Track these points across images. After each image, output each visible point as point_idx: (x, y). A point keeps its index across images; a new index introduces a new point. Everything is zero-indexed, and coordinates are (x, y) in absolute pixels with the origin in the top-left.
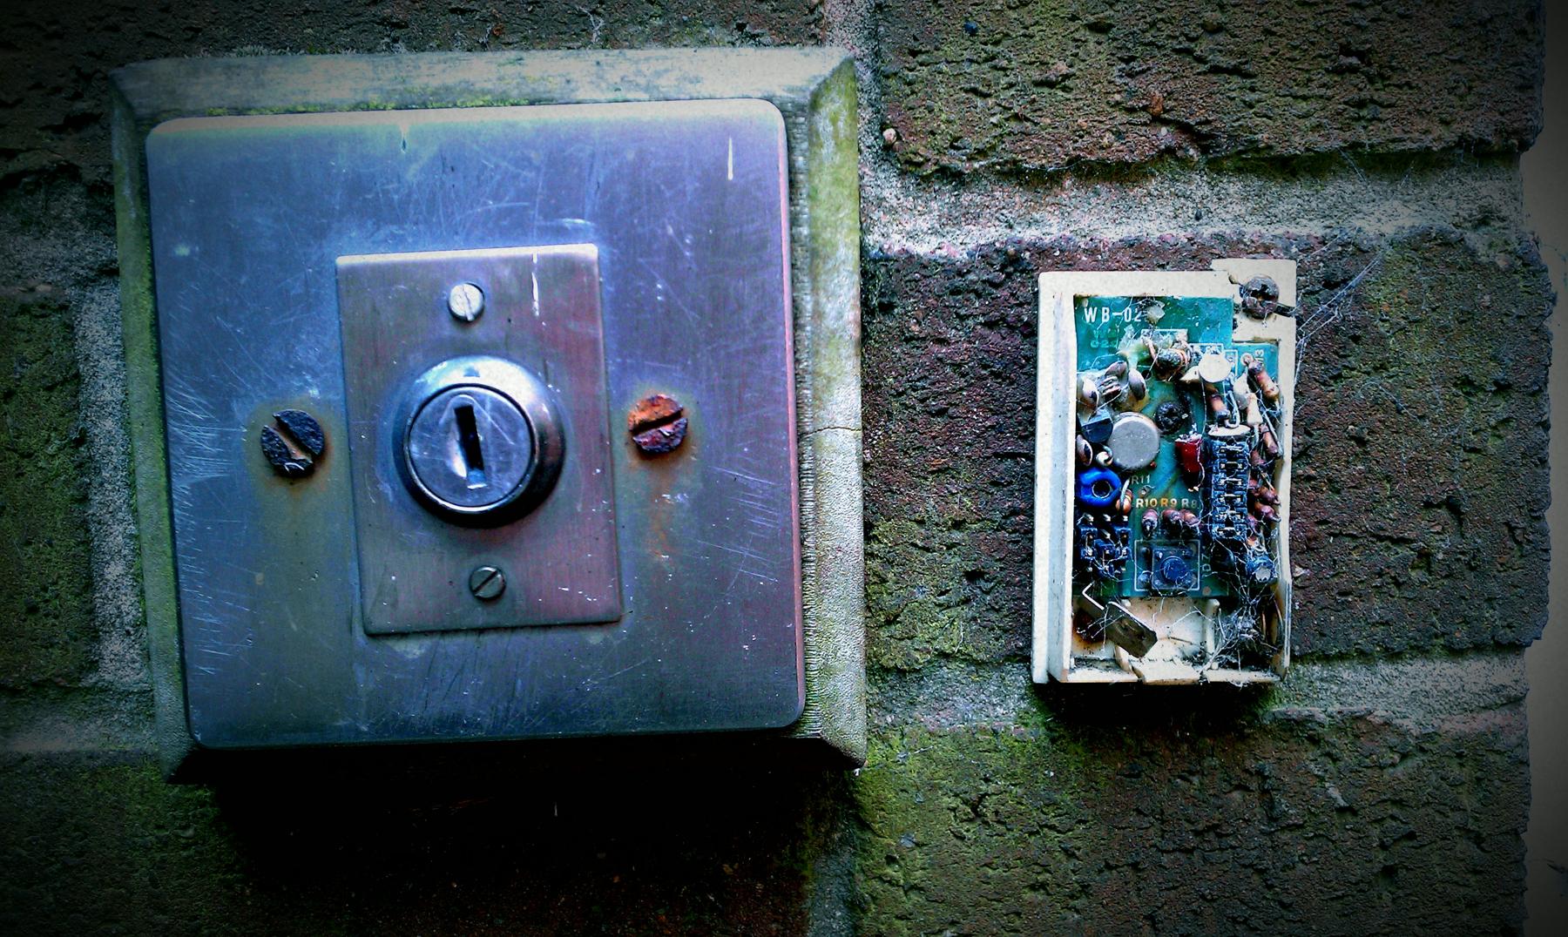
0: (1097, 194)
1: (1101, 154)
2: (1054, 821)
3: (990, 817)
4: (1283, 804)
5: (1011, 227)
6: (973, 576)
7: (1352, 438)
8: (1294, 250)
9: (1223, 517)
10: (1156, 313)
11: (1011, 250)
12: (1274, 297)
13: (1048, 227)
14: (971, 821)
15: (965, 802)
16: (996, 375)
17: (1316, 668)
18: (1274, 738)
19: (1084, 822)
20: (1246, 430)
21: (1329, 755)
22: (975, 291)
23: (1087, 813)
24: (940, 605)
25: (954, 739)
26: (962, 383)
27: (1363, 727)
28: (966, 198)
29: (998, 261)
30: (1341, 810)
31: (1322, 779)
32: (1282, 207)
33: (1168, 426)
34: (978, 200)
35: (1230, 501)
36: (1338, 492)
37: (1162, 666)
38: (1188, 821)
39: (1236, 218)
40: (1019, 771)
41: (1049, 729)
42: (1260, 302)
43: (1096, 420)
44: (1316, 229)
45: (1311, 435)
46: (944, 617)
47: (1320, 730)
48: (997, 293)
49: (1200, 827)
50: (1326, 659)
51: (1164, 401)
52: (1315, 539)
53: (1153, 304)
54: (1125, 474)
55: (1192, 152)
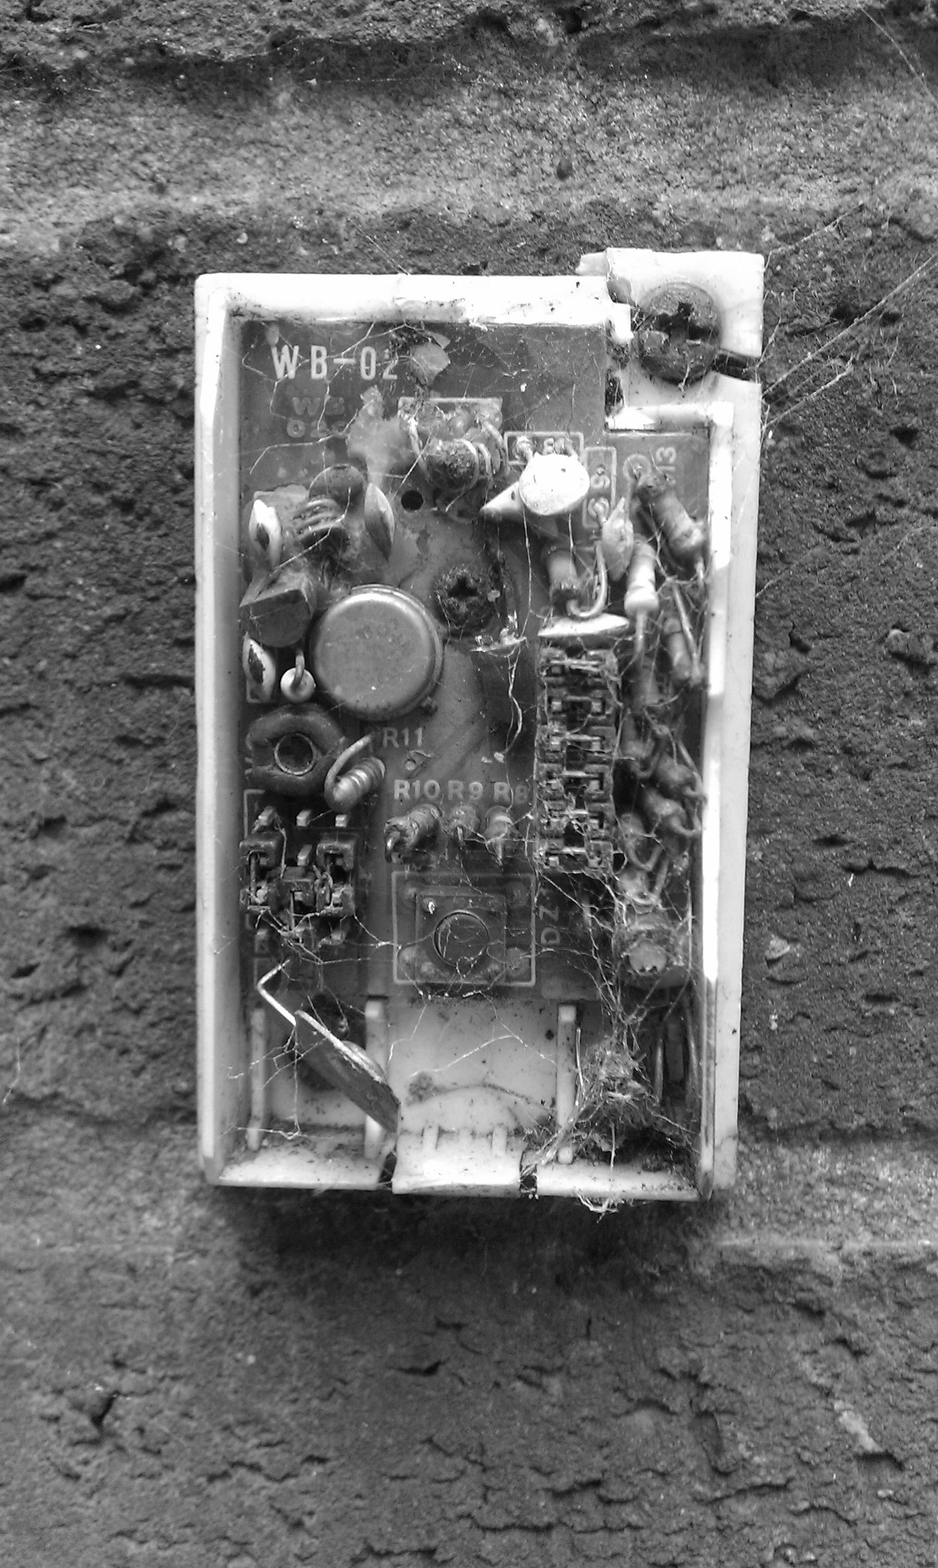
0: (346, 122)
1: (339, 26)
2: (257, 1456)
3: (129, 1437)
4: (741, 1444)
5: (161, 189)
6: (87, 936)
7: (898, 656)
8: (767, 236)
9: (558, 823)
10: (432, 360)
11: (145, 230)
12: (712, 333)
13: (244, 189)
14: (95, 1443)
15: (78, 1407)
16: (126, 506)
17: (820, 1157)
18: (723, 1303)
19: (322, 1460)
20: (613, 623)
21: (843, 1342)
22: (69, 321)
23: (326, 1444)
24: (18, 997)
25: (48, 1275)
26: (52, 522)
27: (918, 1287)
28: (67, 129)
29: (121, 257)
30: (869, 1459)
31: (827, 1393)
32: (751, 149)
33: (456, 618)
34: (92, 132)
35: (572, 785)
36: (866, 777)
37: (453, 1160)
38: (537, 1469)
39: (647, 175)
40: (182, 1350)
41: (244, 1265)
42: (680, 341)
43: (273, 593)
44: (822, 195)
45: (804, 650)
46: (28, 1021)
47: (822, 1291)
48: (118, 325)
49: (562, 1483)
50: (839, 1137)
51: (452, 562)
52: (814, 877)
53: (422, 341)
54: (353, 723)
55: (542, 25)
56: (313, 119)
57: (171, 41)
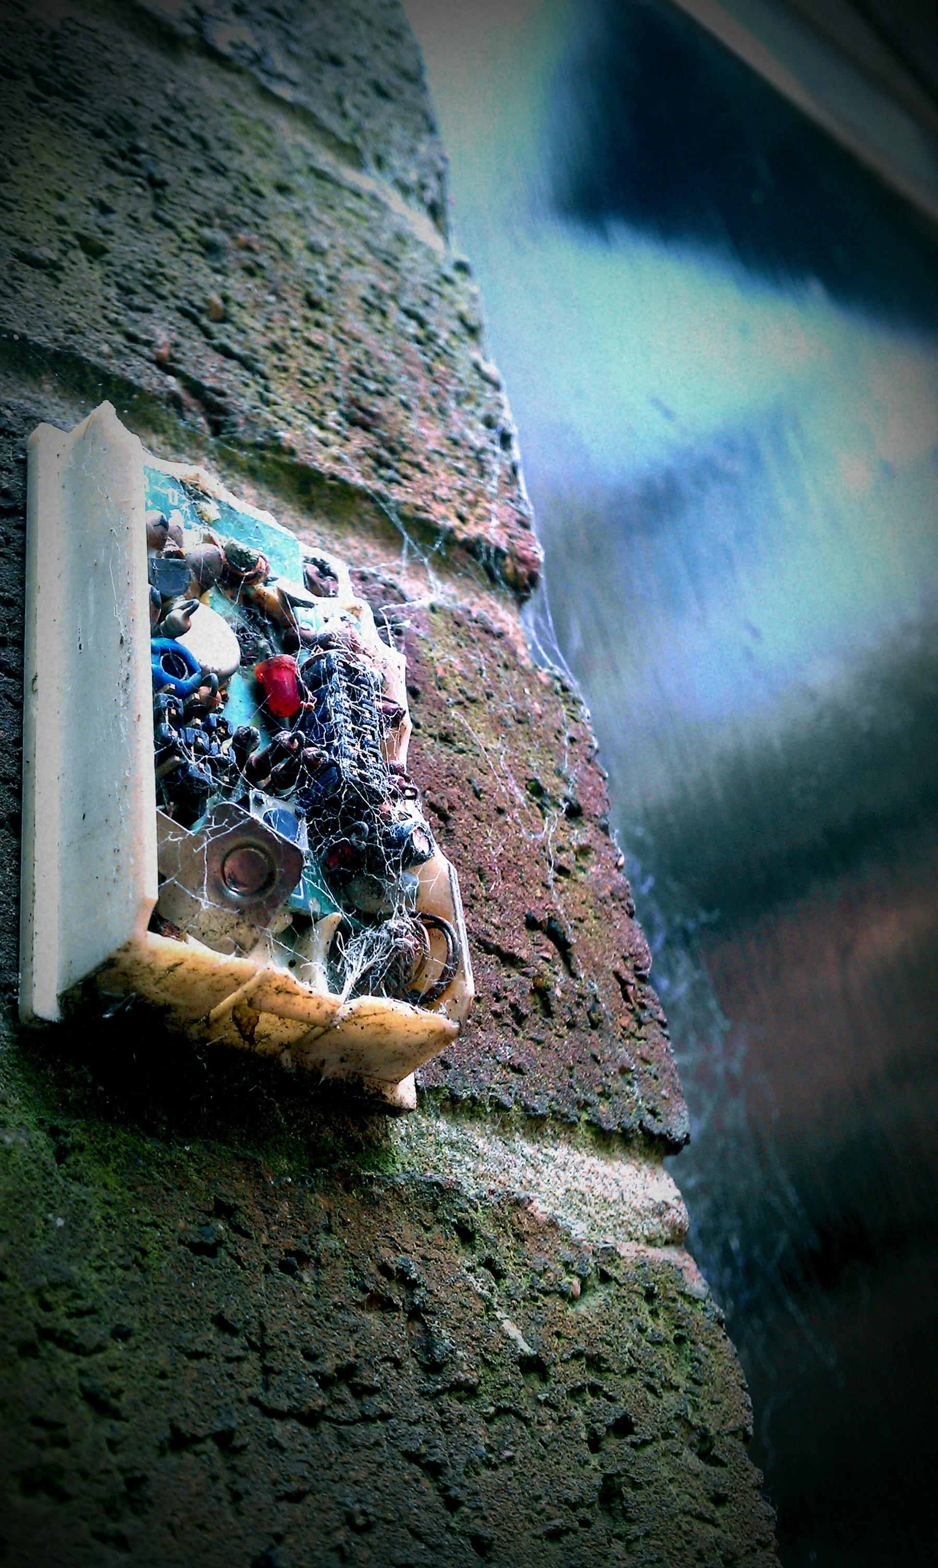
56: (66, 405)
57: (47, 285)
